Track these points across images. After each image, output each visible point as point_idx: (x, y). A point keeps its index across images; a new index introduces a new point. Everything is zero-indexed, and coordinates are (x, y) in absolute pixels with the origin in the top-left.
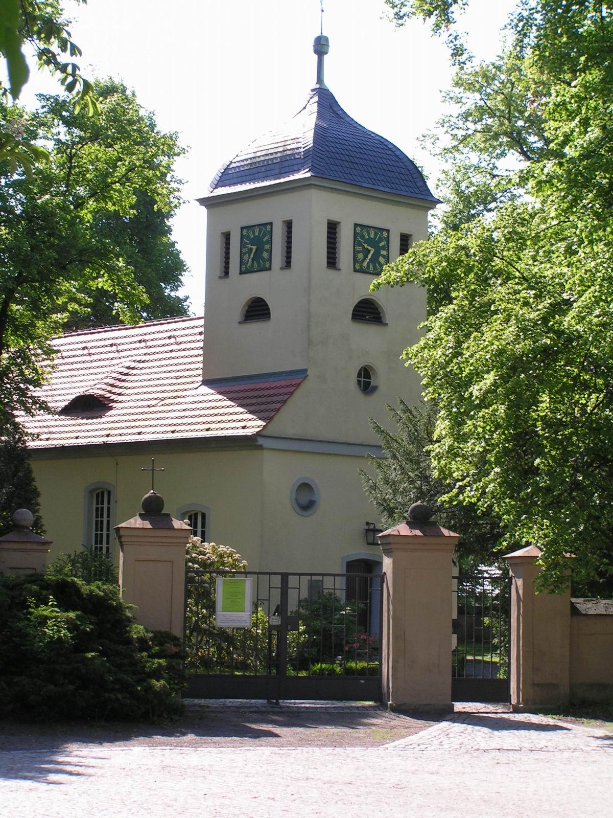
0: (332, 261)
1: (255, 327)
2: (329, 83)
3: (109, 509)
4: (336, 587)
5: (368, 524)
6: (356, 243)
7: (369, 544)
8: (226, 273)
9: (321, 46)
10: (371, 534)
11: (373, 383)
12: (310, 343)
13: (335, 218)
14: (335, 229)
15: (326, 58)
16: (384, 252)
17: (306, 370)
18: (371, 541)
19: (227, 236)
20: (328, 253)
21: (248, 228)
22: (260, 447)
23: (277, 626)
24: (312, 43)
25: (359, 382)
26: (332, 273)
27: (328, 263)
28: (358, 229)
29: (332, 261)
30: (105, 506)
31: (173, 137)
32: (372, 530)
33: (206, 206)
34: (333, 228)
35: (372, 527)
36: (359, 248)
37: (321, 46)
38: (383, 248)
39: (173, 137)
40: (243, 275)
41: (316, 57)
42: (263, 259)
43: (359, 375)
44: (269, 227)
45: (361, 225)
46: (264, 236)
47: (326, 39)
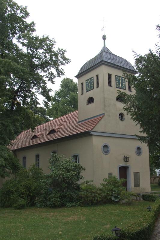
0: (110, 84)
1: (91, 105)
2: (106, 46)
3: (78, 161)
4: (116, 174)
5: (124, 156)
6: (116, 80)
7: (125, 162)
8: (83, 93)
9: (104, 38)
10: (126, 159)
11: (123, 118)
12: (105, 106)
13: (110, 73)
14: (110, 76)
15: (106, 40)
16: (124, 83)
17: (104, 113)
18: (126, 161)
19: (82, 84)
20: (109, 81)
21: (87, 80)
22: (92, 135)
23: (147, 136)
24: (102, 37)
25: (120, 117)
26: (110, 88)
27: (109, 85)
28: (117, 77)
29: (110, 84)
30: (77, 160)
31: (63, 52)
32: (126, 158)
33: (77, 78)
34: (110, 76)
35: (126, 157)
36: (117, 82)
37: (104, 38)
38: (124, 82)
39: (63, 52)
40: (87, 92)
41: (103, 40)
42: (92, 87)
43: (119, 116)
44: (92, 78)
45: (118, 76)
46: (91, 81)
47: (105, 35)
